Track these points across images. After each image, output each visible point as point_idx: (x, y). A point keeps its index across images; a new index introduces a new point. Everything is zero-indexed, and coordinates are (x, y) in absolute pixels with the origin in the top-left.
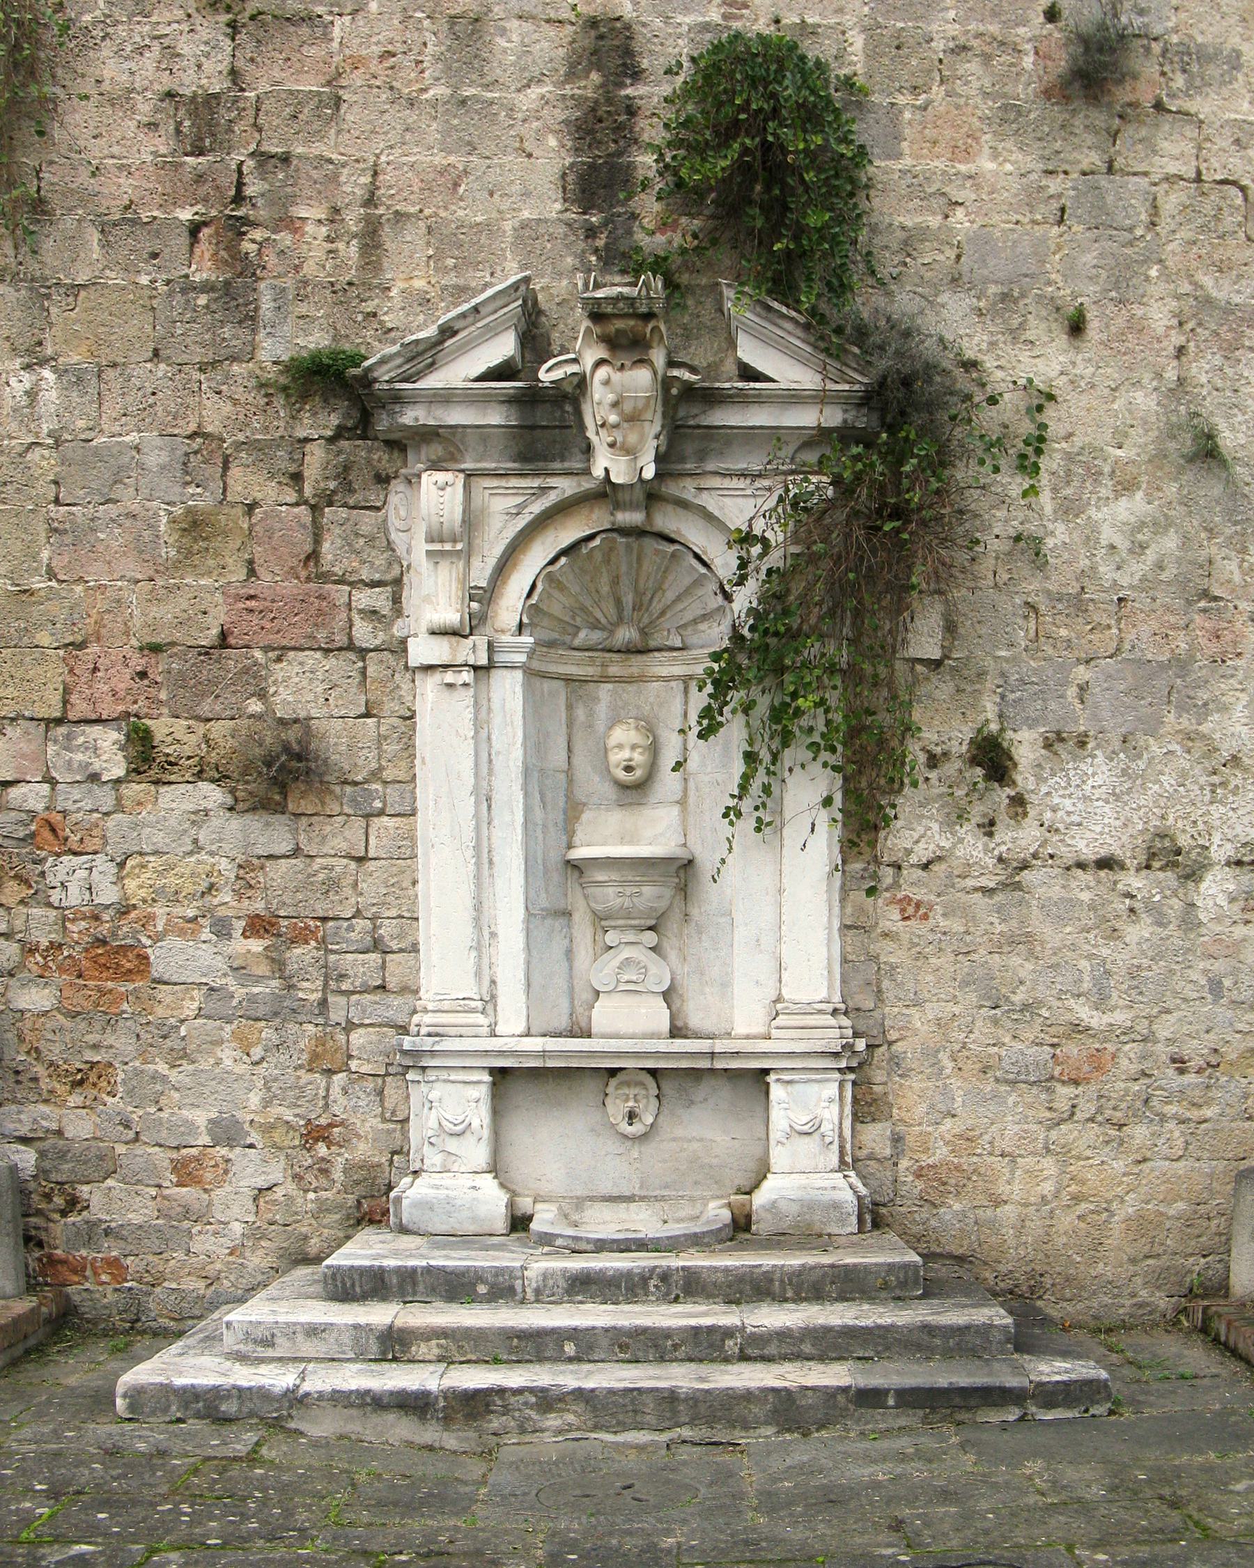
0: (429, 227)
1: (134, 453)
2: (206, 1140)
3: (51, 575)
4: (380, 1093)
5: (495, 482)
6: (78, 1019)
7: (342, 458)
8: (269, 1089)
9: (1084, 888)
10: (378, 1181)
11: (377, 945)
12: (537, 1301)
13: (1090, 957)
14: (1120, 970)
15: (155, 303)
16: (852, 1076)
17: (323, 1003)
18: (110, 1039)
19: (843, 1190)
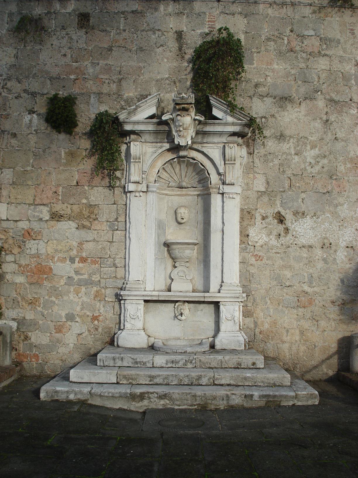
9: (304, 254)
13: (307, 272)
14: (315, 275)
16: (242, 304)
19: (241, 338)
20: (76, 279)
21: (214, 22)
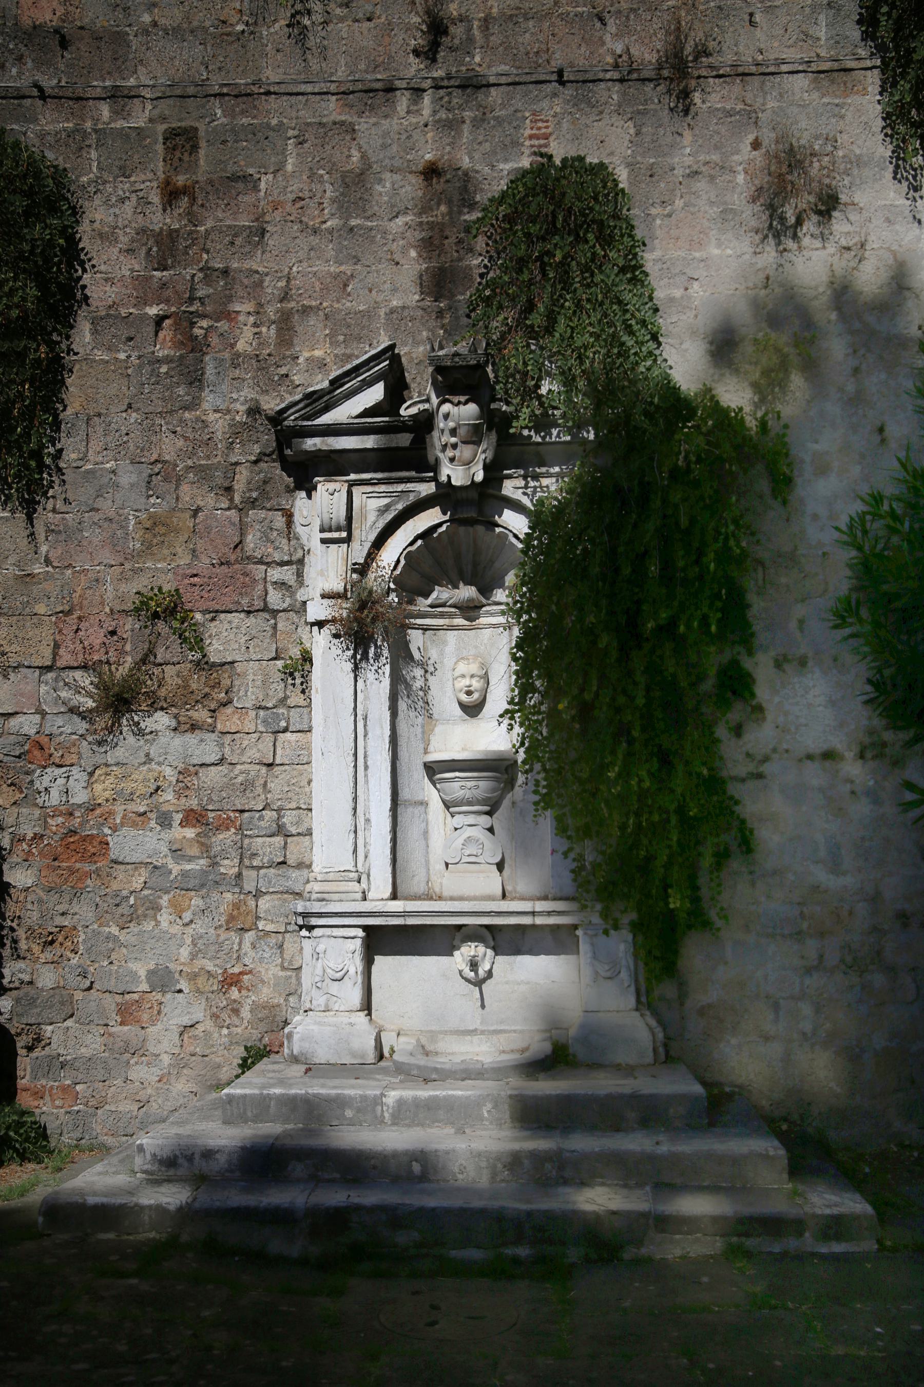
0: (326, 315)
1: (112, 476)
2: (145, 987)
3: (48, 562)
4: (281, 946)
5: (369, 489)
6: (53, 892)
7: (262, 475)
8: (195, 945)
10: (278, 1018)
11: (280, 830)
12: (393, 1124)
15: (130, 371)
17: (239, 875)
18: (75, 908)
20: (175, 873)
21: (546, 137)
